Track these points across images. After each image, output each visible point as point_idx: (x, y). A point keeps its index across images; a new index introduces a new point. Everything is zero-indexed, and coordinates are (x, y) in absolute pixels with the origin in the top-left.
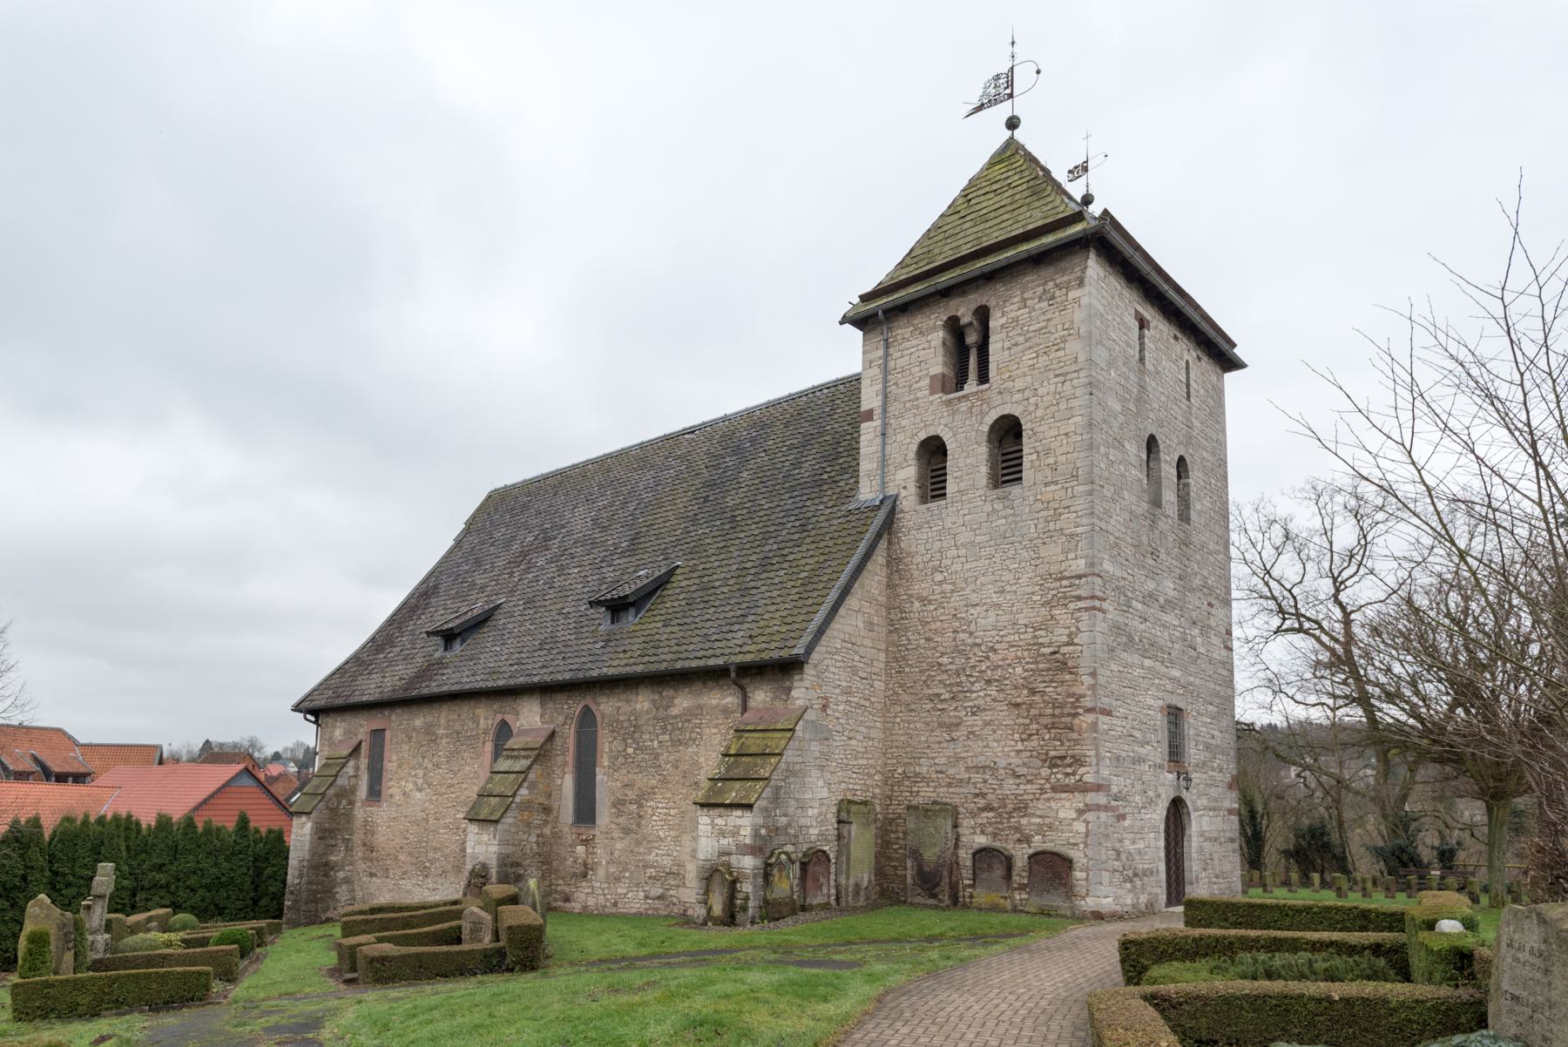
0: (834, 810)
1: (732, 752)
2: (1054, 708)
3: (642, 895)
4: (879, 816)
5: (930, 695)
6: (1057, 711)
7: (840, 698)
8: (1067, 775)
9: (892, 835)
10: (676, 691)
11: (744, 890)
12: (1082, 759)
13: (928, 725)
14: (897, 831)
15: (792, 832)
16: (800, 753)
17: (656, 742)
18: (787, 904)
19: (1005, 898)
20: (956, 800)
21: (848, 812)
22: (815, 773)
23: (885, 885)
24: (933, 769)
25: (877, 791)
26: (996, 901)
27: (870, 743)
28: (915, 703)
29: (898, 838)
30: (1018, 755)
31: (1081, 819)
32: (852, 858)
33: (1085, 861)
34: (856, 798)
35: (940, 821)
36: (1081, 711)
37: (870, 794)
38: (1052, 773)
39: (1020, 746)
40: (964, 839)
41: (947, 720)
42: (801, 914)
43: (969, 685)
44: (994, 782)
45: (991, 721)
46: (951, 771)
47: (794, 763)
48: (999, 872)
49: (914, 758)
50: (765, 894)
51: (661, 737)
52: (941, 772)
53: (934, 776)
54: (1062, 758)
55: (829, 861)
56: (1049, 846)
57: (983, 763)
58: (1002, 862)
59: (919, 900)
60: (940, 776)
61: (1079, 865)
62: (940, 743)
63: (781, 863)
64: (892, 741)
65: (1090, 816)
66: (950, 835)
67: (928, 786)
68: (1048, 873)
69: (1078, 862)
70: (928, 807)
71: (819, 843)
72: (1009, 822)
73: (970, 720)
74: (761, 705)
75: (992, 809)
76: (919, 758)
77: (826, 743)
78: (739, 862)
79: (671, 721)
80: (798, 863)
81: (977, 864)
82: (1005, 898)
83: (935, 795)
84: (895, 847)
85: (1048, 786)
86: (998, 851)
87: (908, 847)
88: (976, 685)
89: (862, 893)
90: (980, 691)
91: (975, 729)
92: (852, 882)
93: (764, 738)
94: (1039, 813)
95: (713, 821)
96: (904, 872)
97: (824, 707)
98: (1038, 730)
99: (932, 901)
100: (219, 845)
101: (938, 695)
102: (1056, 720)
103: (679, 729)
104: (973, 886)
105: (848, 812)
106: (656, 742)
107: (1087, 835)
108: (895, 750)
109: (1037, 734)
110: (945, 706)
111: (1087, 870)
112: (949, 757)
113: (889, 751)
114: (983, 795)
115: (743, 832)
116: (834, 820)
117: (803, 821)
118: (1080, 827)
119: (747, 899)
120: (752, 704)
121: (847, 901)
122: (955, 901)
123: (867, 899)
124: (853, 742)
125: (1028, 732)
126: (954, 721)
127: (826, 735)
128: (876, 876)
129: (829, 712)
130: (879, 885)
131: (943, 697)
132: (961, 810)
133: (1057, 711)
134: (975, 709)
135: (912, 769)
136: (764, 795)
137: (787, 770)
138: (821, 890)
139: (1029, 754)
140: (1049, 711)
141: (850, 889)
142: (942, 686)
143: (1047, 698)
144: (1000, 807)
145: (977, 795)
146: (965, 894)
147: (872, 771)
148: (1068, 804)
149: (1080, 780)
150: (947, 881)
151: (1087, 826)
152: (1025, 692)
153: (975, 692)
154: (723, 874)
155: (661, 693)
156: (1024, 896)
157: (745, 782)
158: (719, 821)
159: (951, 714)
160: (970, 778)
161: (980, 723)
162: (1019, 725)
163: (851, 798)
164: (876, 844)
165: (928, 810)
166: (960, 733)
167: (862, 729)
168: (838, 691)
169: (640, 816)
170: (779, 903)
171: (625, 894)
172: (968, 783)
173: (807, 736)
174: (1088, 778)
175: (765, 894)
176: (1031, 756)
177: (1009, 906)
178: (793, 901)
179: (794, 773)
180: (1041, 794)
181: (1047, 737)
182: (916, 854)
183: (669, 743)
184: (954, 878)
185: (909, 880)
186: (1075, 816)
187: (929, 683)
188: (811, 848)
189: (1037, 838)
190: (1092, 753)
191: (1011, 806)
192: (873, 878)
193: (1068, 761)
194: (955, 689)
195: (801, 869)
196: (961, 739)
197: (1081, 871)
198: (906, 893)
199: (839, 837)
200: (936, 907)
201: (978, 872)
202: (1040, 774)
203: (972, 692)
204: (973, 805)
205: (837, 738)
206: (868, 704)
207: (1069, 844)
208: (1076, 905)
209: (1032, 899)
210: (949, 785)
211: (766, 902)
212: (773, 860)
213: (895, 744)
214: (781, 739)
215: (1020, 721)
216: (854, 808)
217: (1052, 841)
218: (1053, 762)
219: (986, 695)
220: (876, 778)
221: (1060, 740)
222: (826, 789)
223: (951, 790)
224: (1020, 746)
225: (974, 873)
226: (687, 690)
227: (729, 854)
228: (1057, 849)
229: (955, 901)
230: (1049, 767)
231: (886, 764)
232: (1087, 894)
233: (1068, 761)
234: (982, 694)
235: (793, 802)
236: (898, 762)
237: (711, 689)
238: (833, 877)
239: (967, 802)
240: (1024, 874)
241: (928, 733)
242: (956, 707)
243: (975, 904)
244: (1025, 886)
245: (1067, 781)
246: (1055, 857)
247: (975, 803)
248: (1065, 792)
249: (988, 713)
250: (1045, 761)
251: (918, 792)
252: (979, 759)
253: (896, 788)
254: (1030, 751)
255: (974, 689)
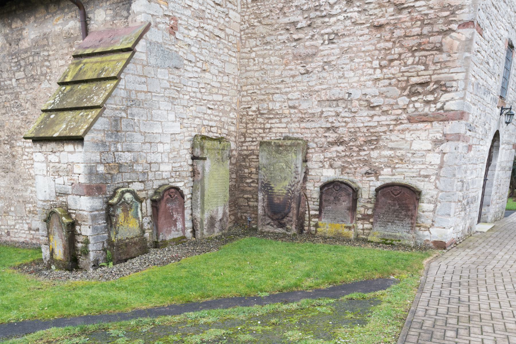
0: (188, 145)
1: (68, 79)
2: (423, 25)
3: (26, 226)
4: (234, 153)
5: (286, 24)
6: (426, 30)
7: (191, 21)
8: (428, 102)
9: (246, 171)
10: (23, 21)
11: (83, 233)
12: (448, 84)
13: (283, 58)
14: (250, 166)
15: (140, 168)
16: (144, 79)
17: (14, 80)
18: (135, 243)
19: (349, 228)
20: (307, 135)
21: (202, 148)
22: (164, 105)
23: (239, 215)
24: (286, 104)
25: (233, 128)
26: (340, 230)
27: (226, 79)
28: (270, 35)
29: (251, 173)
30: (375, 84)
31: (437, 150)
32: (206, 193)
33: (434, 193)
34: (211, 135)
35: (291, 156)
36: (454, 26)
37: (226, 132)
38: (410, 103)
39: (378, 74)
40: (312, 173)
41: (303, 51)
42: (152, 251)
43: (328, 8)
44: (346, 115)
45: (350, 48)
46: (304, 106)
47: (137, 92)
48: (345, 203)
49: (267, 94)
50: (109, 236)
51: (17, 74)
52: (294, 107)
53: (287, 111)
54: (423, 84)
55: (183, 196)
56: (398, 179)
57: (337, 96)
58: (349, 195)
59: (269, 228)
60: (292, 111)
61: (428, 196)
62: (293, 76)
63: (125, 202)
64: (246, 78)
65: (446, 147)
66: (300, 169)
67: (281, 122)
68: (394, 205)
69: (428, 193)
70: (280, 142)
71: (172, 180)
72: (359, 155)
73: (326, 49)
74: (102, 28)
75: (342, 143)
76: (273, 94)
77: (176, 72)
78: (76, 203)
79: (23, 56)
80: (149, 201)
81: (324, 197)
82: (349, 228)
83: (286, 130)
84: (248, 181)
85: (404, 116)
86: (346, 184)
87: (260, 181)
88: (336, 7)
89: (217, 225)
90: (340, 14)
91: (331, 58)
92: (206, 215)
93: (101, 62)
94: (391, 145)
95: (46, 158)
96: (255, 204)
97: (173, 29)
98: (400, 54)
99: (280, 230)
100: (272, 169)
101: (294, 23)
102: (424, 40)
103: (31, 64)
104: (319, 216)
105: (202, 148)
106: (14, 80)
107: (441, 167)
108: (249, 87)
109: (399, 59)
110: (301, 35)
111: (435, 202)
112: (302, 91)
113: (244, 88)
114: (333, 129)
115: (76, 170)
116: (188, 156)
117: (151, 158)
118: (435, 158)
119: (87, 242)
120: (93, 26)
121: (203, 234)
122: (301, 227)
123: (222, 229)
124: (207, 75)
125: (389, 57)
126: (310, 51)
127: (175, 63)
128: (230, 207)
129: (178, 35)
130: (232, 215)
131: (299, 26)
132: (312, 145)
133: (426, 30)
134: (332, 36)
135: (265, 106)
136: (97, 126)
137: (128, 99)
138: (175, 225)
139: (387, 82)
140: (416, 30)
141: (205, 223)
142: (299, 12)
143: (415, 14)
144: (350, 140)
145: (328, 129)
146: (310, 224)
147: (227, 108)
148: (423, 135)
149: (442, 108)
150: (295, 212)
151: (442, 158)
152: (391, 10)
153: (333, 16)
154: (59, 217)
155: (10, 25)
156: (368, 226)
157: (78, 112)
158: (53, 158)
159: (307, 43)
160: (322, 112)
161: (337, 51)
162: (380, 51)
163: (205, 134)
164: (231, 178)
165: (280, 146)
166: (314, 65)
167: (216, 62)
168: (188, 12)
169: (14, 156)
170: (126, 245)
171: (14, 226)
172: (321, 117)
173: (152, 61)
174: (451, 106)
175: (109, 236)
176: (390, 84)
177: (352, 236)
178: (143, 240)
179: (138, 104)
180: (395, 125)
181: (410, 61)
182: (267, 188)
183: (25, 80)
184: (301, 210)
185: (260, 211)
186: (430, 147)
187: (286, 10)
188: (164, 185)
189: (387, 171)
190: (461, 76)
191: (362, 139)
192: (227, 211)
193: (431, 87)
194: (312, 15)
195: (153, 206)
196: (315, 71)
197: (430, 202)
198: (257, 221)
199: (194, 173)
200: (284, 236)
201: (324, 203)
202: (397, 103)
203: (331, 16)
204: (323, 139)
205: (188, 68)
206: (222, 35)
207: (420, 176)
208: (418, 235)
209: (375, 229)
210: (301, 120)
211: (110, 242)
212: (115, 200)
213: (250, 81)
214: (118, 61)
215: (382, 45)
216: (208, 144)
217: (401, 173)
218: (414, 89)
219: (346, 18)
220: (232, 115)
221: (425, 64)
222: (178, 124)
223: (303, 125)
224: (378, 74)
225: (321, 204)
226: (32, 19)
227: (66, 194)
228: (407, 181)
229: (301, 227)
230: (408, 96)
231: (241, 102)
232: (433, 225)
233: (431, 87)
234: (341, 17)
235: (138, 137)
236: (253, 100)
237: (54, 14)
238: (187, 212)
239: (317, 137)
240: (369, 205)
241: (282, 67)
242: (313, 36)
243: (319, 233)
244: (370, 216)
245: (427, 110)
246: (404, 190)
247: (326, 137)
248: (423, 121)
249: (347, 39)
250: (404, 89)
251: (270, 129)
252: (333, 91)
253: (250, 126)
254: (389, 79)
255: (333, 12)
